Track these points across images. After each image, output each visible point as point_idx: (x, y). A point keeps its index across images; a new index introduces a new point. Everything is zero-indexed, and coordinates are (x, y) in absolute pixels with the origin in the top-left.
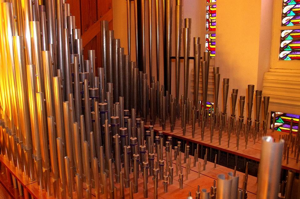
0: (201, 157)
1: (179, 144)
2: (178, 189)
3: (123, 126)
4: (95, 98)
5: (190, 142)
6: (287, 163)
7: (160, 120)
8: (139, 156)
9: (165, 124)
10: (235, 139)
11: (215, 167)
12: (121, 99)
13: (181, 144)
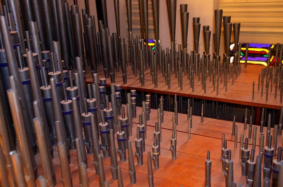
0: (182, 112)
1: (148, 98)
2: (171, 160)
3: (251, 120)
4: (18, 47)
5: (165, 95)
6: (217, 94)
7: (105, 69)
8: (124, 134)
9: (114, 74)
10: (176, 80)
11: (202, 121)
12: (56, 44)
13: (151, 98)
